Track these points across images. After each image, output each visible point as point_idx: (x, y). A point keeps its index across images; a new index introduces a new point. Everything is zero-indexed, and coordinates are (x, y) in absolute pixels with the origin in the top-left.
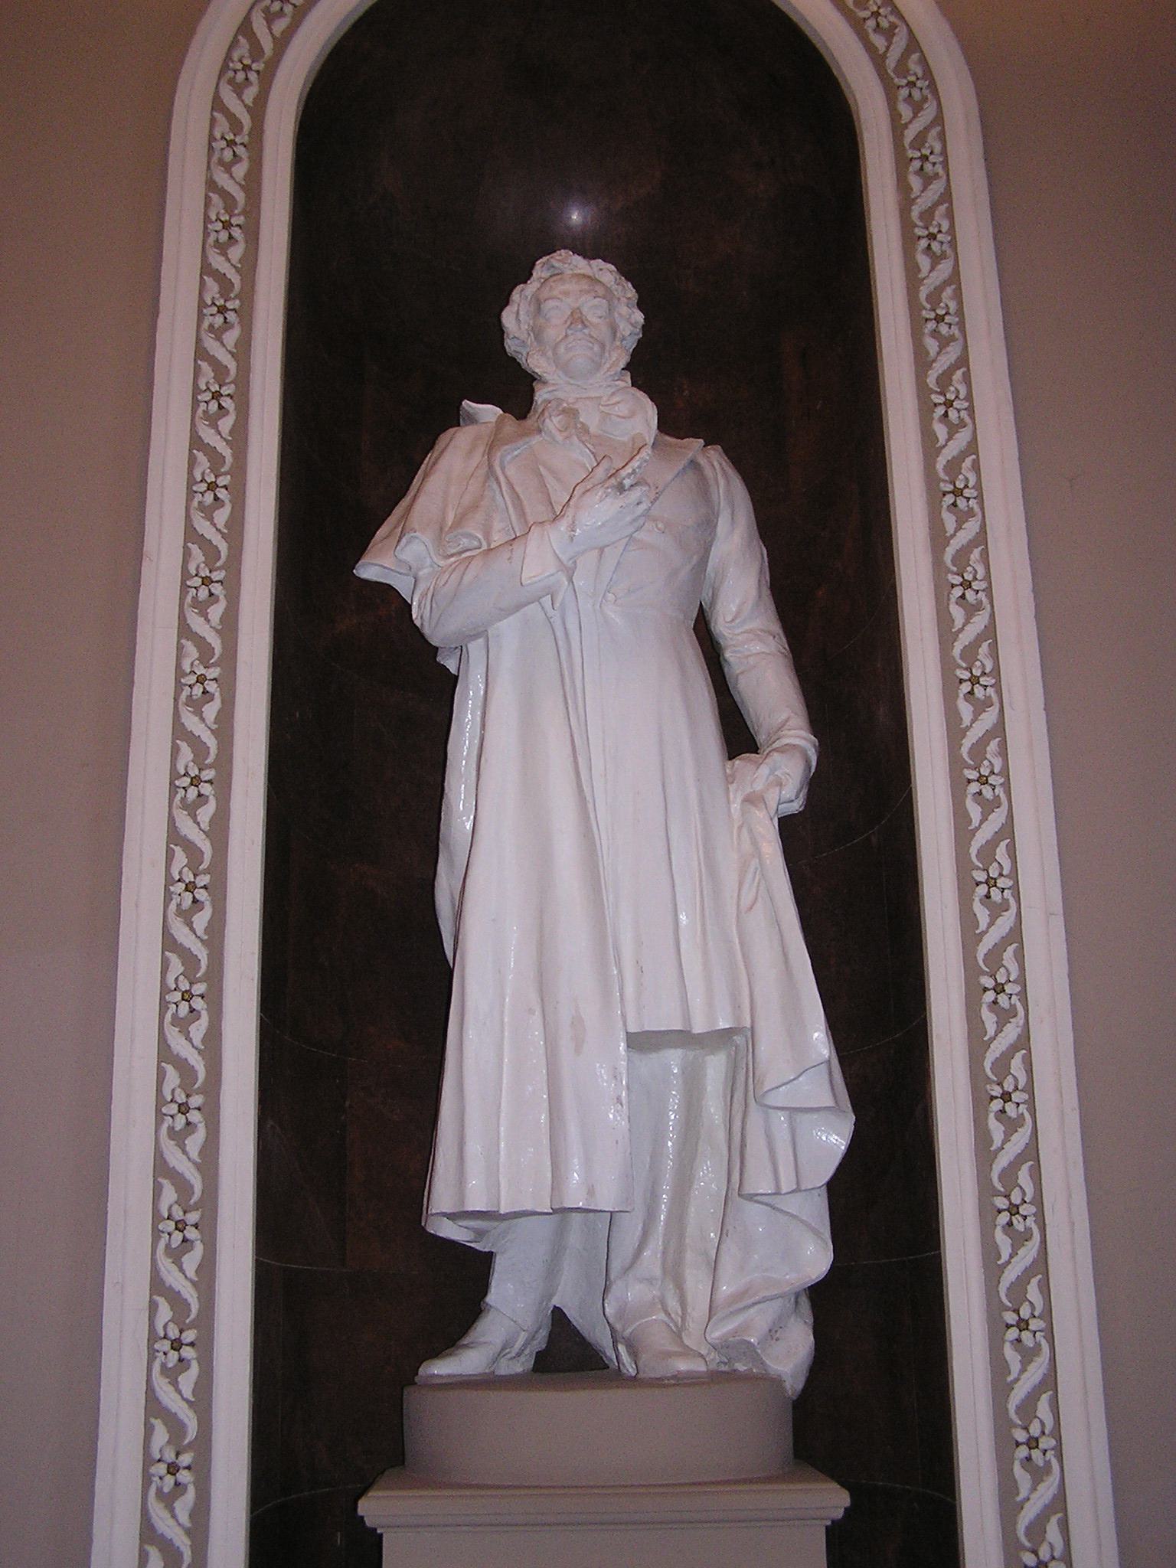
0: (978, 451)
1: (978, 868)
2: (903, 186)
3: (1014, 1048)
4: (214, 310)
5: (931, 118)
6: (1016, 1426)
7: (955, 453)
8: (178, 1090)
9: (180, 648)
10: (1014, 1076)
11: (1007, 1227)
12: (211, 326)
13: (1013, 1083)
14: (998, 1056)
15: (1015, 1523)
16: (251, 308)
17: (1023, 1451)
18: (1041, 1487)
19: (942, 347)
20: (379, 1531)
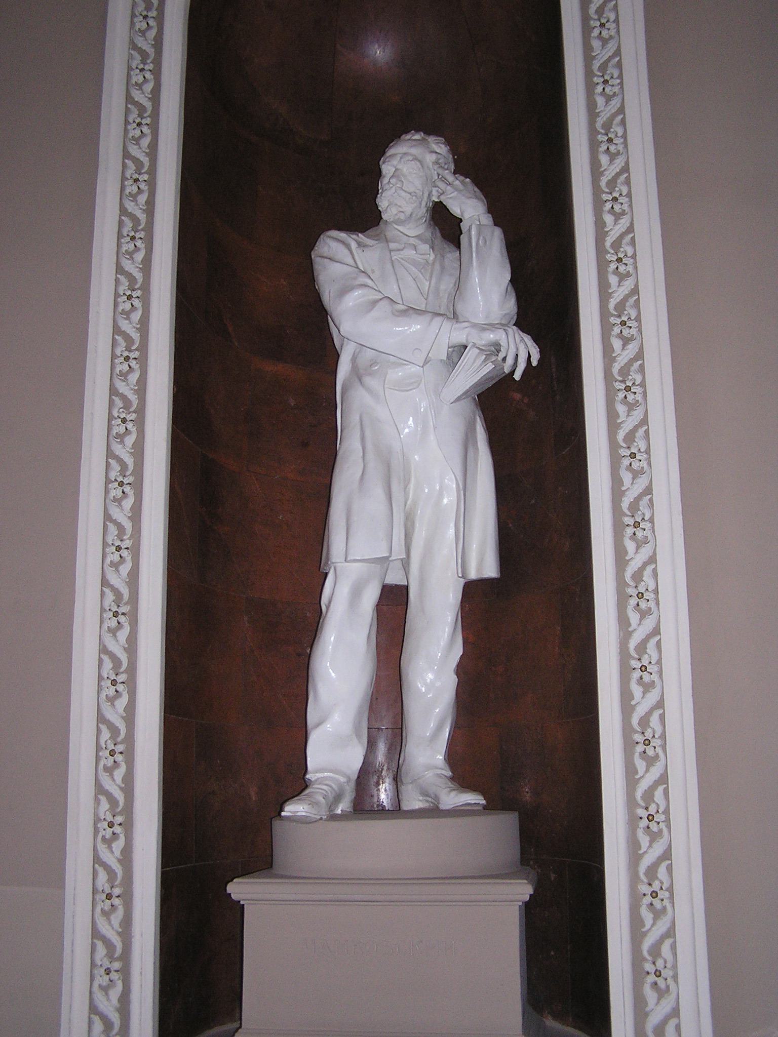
1: (637, 732)
2: (623, 621)
3: (657, 783)
4: (135, 125)
5: (612, 51)
7: (626, 361)
8: (109, 741)
9: (108, 465)
10: (657, 804)
13: (656, 808)
16: (155, 178)
17: (651, 978)
18: (648, 695)
19: (651, 842)
20: (242, 903)
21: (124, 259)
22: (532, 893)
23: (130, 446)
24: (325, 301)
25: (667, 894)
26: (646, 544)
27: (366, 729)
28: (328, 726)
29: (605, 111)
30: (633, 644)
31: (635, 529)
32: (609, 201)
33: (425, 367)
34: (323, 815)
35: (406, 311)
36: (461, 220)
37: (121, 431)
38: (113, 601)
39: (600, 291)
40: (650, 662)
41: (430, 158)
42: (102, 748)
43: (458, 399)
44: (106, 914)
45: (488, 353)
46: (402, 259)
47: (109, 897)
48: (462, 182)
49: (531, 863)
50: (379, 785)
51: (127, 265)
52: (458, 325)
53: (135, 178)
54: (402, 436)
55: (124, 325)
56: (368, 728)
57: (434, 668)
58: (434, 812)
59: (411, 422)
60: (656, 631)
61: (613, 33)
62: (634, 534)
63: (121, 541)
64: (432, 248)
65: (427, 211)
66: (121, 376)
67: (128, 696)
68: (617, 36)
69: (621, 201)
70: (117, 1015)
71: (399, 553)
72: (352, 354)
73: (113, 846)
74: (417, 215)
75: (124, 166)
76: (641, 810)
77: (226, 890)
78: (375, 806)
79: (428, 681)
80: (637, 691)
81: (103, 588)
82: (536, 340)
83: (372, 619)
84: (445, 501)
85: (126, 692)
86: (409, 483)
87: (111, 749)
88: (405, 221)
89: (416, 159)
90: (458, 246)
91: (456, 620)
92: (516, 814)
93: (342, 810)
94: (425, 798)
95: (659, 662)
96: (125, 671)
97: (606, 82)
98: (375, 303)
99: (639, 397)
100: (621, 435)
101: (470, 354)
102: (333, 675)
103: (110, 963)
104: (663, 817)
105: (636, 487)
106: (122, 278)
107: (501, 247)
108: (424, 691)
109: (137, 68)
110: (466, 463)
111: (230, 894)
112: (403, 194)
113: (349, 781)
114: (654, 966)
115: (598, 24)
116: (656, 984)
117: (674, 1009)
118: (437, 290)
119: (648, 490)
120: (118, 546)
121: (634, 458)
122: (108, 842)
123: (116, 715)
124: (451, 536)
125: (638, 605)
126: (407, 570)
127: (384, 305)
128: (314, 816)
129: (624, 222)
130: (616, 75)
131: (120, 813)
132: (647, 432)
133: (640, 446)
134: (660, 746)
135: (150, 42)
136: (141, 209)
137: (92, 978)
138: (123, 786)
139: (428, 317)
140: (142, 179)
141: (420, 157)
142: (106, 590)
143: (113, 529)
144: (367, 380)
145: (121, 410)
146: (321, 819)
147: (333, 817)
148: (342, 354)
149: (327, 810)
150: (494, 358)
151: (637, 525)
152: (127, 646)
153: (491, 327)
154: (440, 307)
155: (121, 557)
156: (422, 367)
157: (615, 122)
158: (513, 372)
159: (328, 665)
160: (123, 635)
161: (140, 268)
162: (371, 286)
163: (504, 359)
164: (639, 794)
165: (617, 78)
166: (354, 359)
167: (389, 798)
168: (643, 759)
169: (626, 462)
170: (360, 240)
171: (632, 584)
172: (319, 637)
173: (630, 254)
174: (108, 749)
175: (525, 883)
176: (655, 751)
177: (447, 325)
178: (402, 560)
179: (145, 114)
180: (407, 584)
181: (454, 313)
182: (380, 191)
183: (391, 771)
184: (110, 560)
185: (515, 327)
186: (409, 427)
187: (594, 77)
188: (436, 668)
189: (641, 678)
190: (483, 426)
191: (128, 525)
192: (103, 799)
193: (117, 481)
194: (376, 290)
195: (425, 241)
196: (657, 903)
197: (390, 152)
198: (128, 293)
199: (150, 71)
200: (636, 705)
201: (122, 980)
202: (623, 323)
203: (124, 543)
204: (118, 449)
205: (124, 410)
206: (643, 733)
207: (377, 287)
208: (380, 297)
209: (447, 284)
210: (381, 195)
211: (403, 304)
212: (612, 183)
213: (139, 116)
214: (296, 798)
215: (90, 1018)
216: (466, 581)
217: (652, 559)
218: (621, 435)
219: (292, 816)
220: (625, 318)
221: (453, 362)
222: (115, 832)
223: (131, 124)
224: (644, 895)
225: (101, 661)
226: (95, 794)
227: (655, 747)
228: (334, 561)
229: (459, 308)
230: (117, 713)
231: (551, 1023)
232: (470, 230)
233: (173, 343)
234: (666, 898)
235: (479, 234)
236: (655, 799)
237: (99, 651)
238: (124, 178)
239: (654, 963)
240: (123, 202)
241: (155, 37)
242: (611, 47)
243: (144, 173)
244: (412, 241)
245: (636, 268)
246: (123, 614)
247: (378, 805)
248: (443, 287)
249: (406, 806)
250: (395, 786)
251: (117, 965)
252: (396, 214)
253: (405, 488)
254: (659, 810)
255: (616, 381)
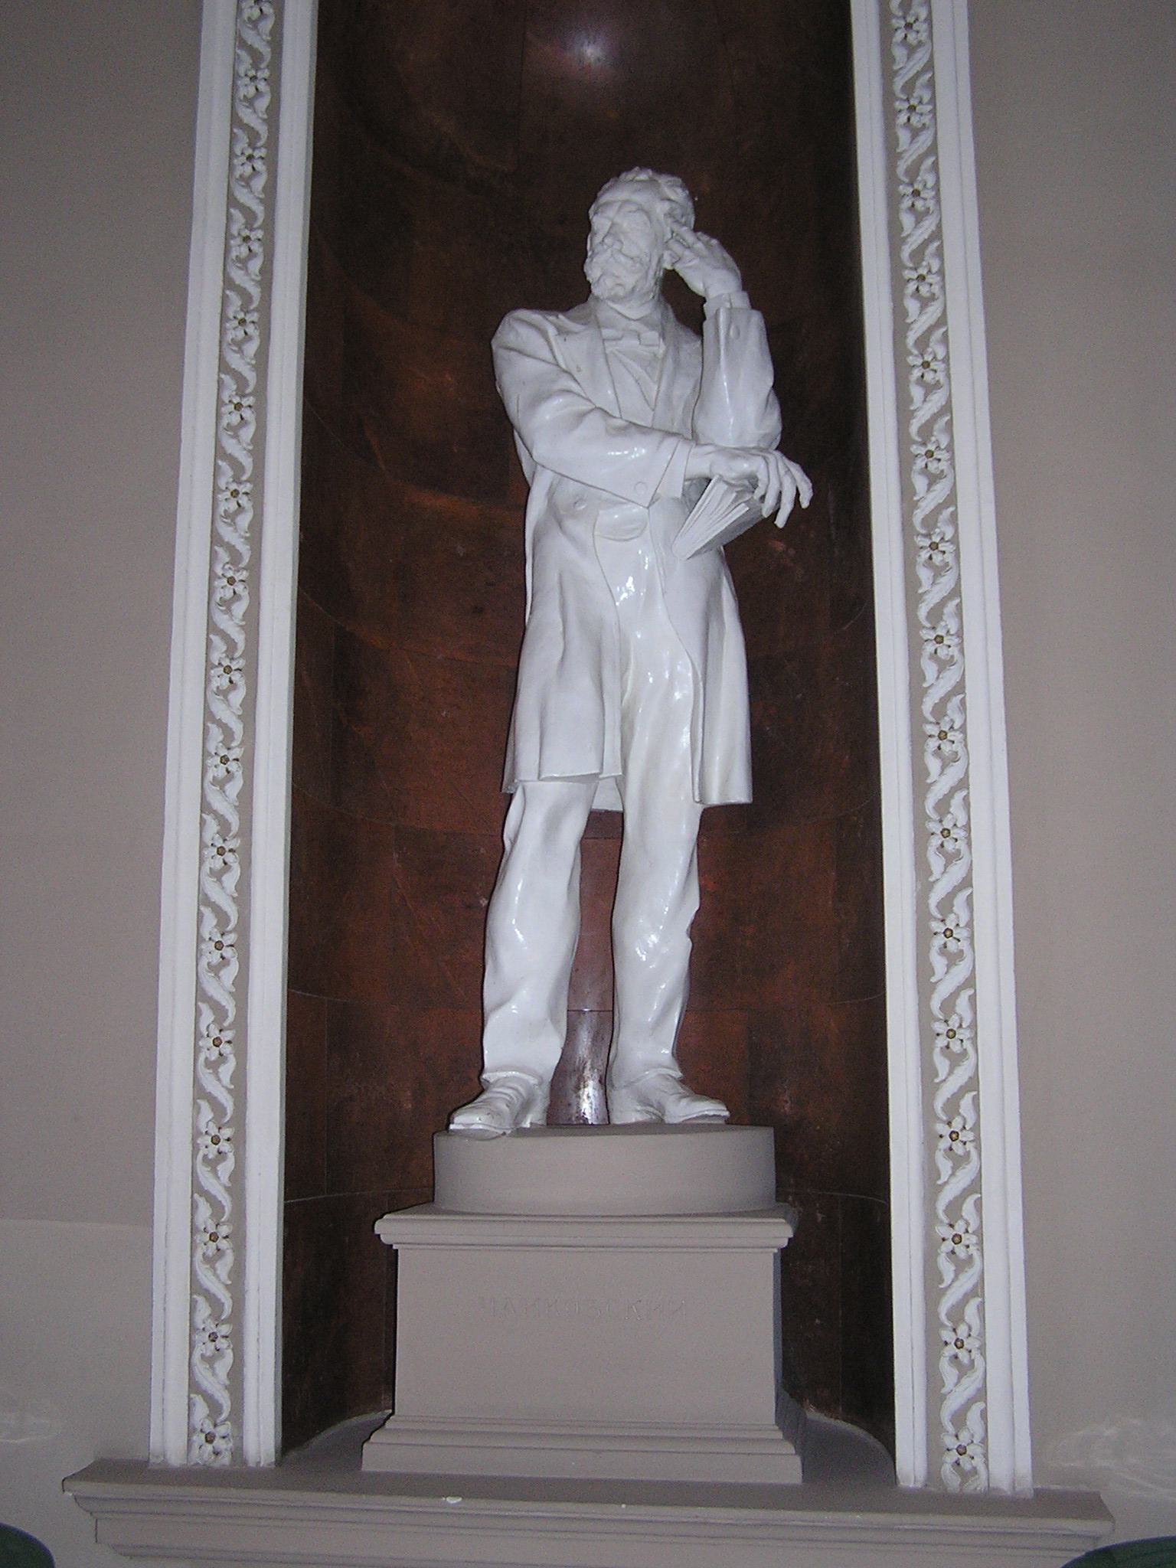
0: (978, 1088)
1: (935, 919)
2: (922, 867)
3: (963, 1090)
4: (236, 322)
5: (922, 64)
6: (939, 1119)
7: (928, 417)
8: (212, 1026)
11: (953, 1358)
12: (205, 1156)
13: (962, 1122)
14: (936, 701)
15: (938, 1314)
17: (951, 1350)
18: (954, 970)
19: (957, 1274)
20: (394, 1247)
21: (230, 351)
22: (791, 1236)
23: (240, 617)
24: (512, 411)
25: (974, 1239)
26: (955, 762)
27: (565, 1012)
28: (513, 1008)
29: (910, 149)
30: (934, 899)
31: (941, 742)
32: (913, 280)
33: (651, 508)
34: (507, 1129)
35: (625, 428)
36: (704, 300)
37: (227, 595)
38: (218, 833)
39: (898, 408)
40: (958, 925)
41: (661, 208)
42: (202, 1036)
43: (697, 553)
44: (210, 1261)
45: (739, 489)
46: (619, 352)
47: (214, 1237)
48: (707, 245)
49: (790, 1198)
50: (579, 1089)
51: (235, 360)
52: (695, 450)
53: (245, 235)
54: (617, 604)
55: (231, 446)
56: (568, 1010)
57: (658, 928)
58: (657, 1126)
59: (630, 583)
60: (967, 882)
61: (923, 36)
62: (939, 748)
63: (229, 749)
64: (663, 336)
65: (656, 284)
66: (226, 518)
67: (238, 965)
68: (929, 41)
69: (931, 281)
70: (226, 1394)
71: (612, 769)
72: (548, 486)
73: (218, 1169)
74: (642, 288)
75: (229, 218)
76: (941, 1125)
77: (373, 1230)
78: (573, 1119)
79: (651, 946)
80: (939, 963)
81: (203, 815)
82: (807, 471)
83: (575, 859)
84: (677, 695)
85: (235, 958)
86: (627, 669)
87: (215, 1037)
88: (625, 297)
89: (641, 209)
90: (700, 333)
91: (691, 861)
92: (771, 1130)
93: (531, 1123)
94: (644, 1108)
95: (970, 925)
96: (234, 930)
97: (912, 109)
98: (582, 416)
99: (949, 558)
100: (923, 612)
101: (715, 490)
102: (520, 937)
103: (217, 1325)
104: (970, 1136)
105: (941, 682)
106: (226, 378)
107: (761, 336)
108: (644, 959)
109: (246, 75)
110: (707, 634)
111: (379, 1235)
112: (623, 259)
113: (540, 1084)
114: (953, 1333)
115: (903, 23)
116: (956, 1357)
117: (979, 1390)
118: (669, 399)
119: (960, 688)
120: (224, 756)
121: (940, 643)
122: (212, 1164)
123: (225, 803)
124: (685, 744)
125: (942, 845)
126: (622, 790)
127: (595, 421)
128: (493, 1129)
129: (933, 311)
130: (926, 98)
131: (228, 1124)
132: (959, 607)
133: (949, 627)
134: (968, 1039)
135: (264, 37)
136: (253, 280)
137: (192, 1347)
138: (234, 990)
139: (657, 436)
140: (255, 237)
141: (646, 207)
142: (208, 818)
143: (216, 733)
144: (569, 524)
145: (227, 566)
146: (504, 1134)
147: (520, 1132)
148: (534, 484)
149: (511, 1122)
150: (748, 497)
151: (943, 736)
152: (236, 895)
153: (744, 452)
154: (672, 420)
155: (228, 771)
156: (648, 508)
157: (923, 167)
158: (774, 515)
159: (514, 922)
160: (231, 880)
161: (252, 364)
162: (576, 391)
163: (763, 498)
164: (939, 1104)
165: (928, 103)
166: (551, 494)
167: (594, 1107)
168: (946, 1056)
169: (930, 648)
170: (560, 323)
171: (935, 816)
172: (501, 885)
173: (941, 355)
174: (211, 1037)
175: (782, 1223)
176: (962, 1046)
177: (683, 449)
178: (616, 778)
179: (242, 476)
180: (622, 809)
181: (693, 431)
182: (589, 254)
183: (596, 1070)
184: (223, 509)
185: (778, 454)
186: (628, 591)
187: (899, 186)
188: (661, 927)
189: (945, 945)
190: (731, 589)
191: (237, 728)
192: (204, 1105)
193: (222, 666)
194: (583, 397)
195: (652, 326)
196: (960, 1250)
197: (605, 198)
198: (236, 400)
199: (265, 80)
200: (936, 983)
201: (233, 1350)
202: (929, 454)
203: (231, 752)
204: (222, 621)
205: (232, 567)
206: (946, 1021)
207: (585, 393)
208: (590, 408)
209: (684, 388)
210: (592, 260)
211: (621, 418)
212: (918, 255)
213: (249, 145)
214: (470, 1106)
215: (190, 1399)
216: (705, 806)
217: (963, 784)
218: (923, 612)
219: (464, 1130)
220: (931, 447)
221: (690, 500)
222: (221, 1150)
223: (242, 78)
224: (944, 1240)
225: (200, 917)
226: (194, 1099)
227: (962, 1041)
228: (522, 778)
229: (700, 424)
230: (223, 987)
231: (813, 1414)
232: (716, 316)
233: (299, 471)
234: (973, 1245)
235: (730, 321)
236: (963, 1214)
237: (198, 901)
238: (228, 236)
239: (954, 1330)
240: (228, 270)
241: (271, 30)
242: (921, 58)
243: (253, 310)
244: (634, 326)
245: (948, 376)
246: (231, 850)
247: (577, 1117)
248: (677, 392)
249: (617, 1120)
250: (602, 1091)
251: (225, 1329)
252: (612, 289)
253: (622, 678)
254: (966, 1126)
255: (918, 535)
